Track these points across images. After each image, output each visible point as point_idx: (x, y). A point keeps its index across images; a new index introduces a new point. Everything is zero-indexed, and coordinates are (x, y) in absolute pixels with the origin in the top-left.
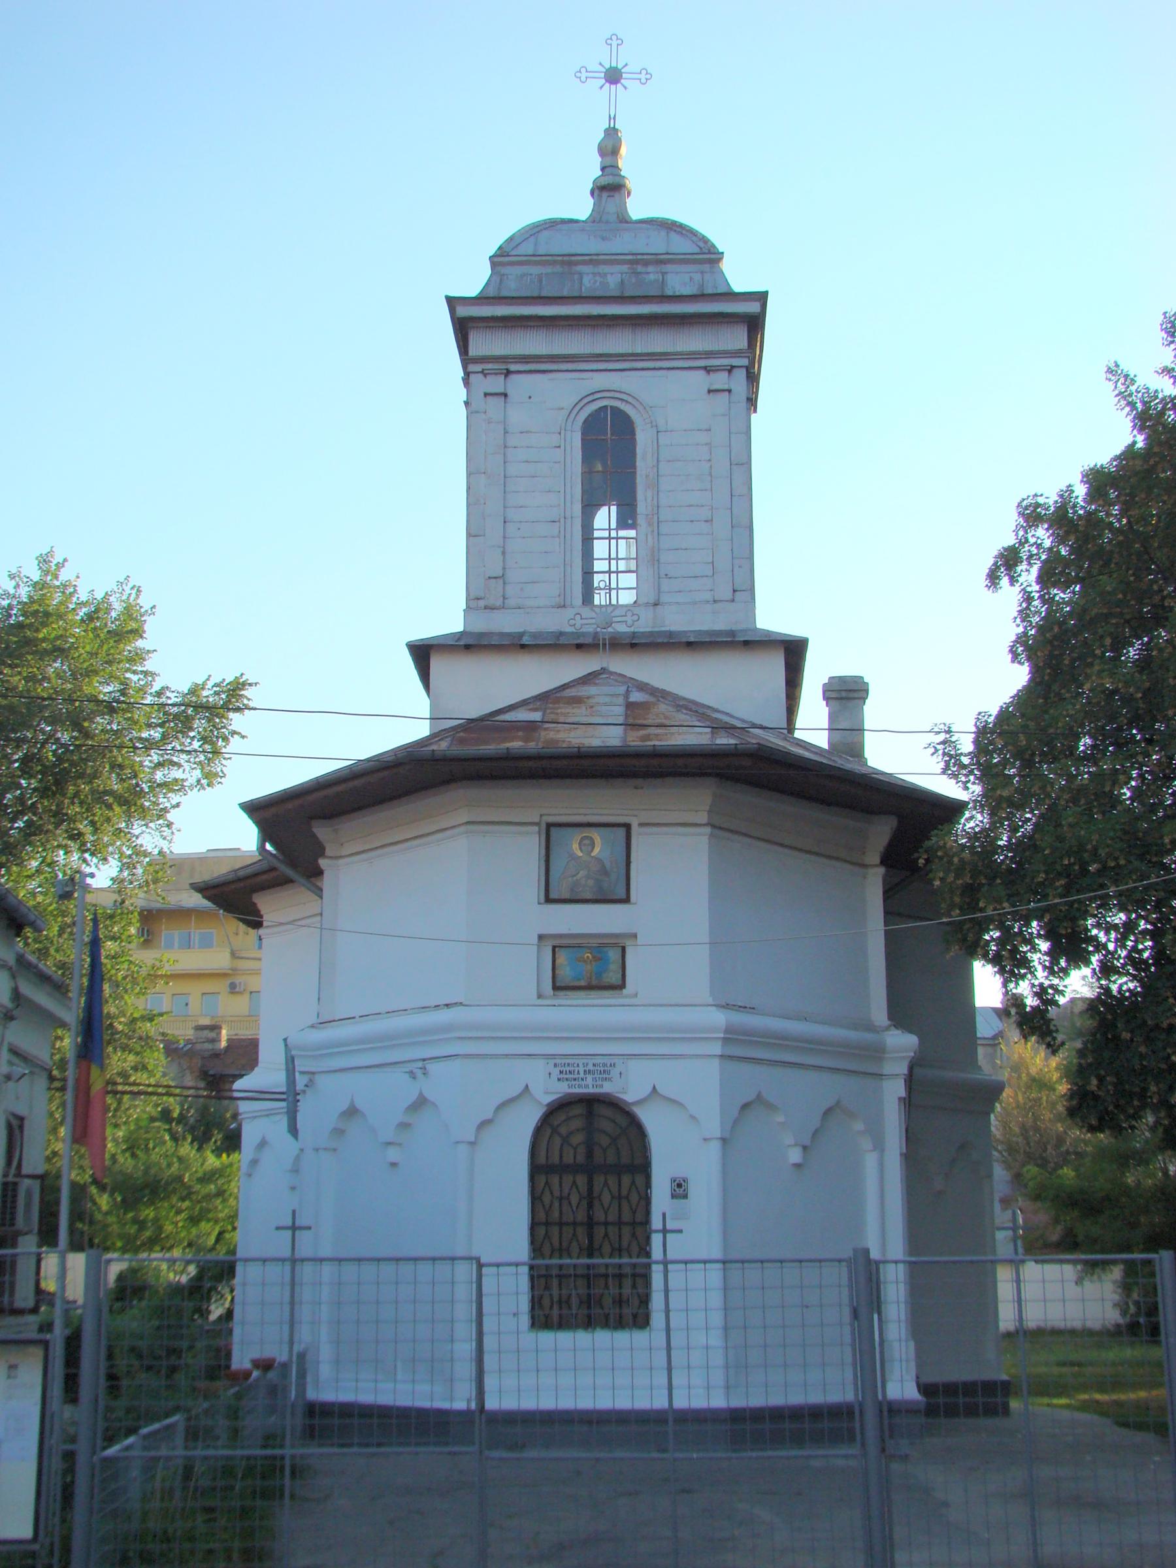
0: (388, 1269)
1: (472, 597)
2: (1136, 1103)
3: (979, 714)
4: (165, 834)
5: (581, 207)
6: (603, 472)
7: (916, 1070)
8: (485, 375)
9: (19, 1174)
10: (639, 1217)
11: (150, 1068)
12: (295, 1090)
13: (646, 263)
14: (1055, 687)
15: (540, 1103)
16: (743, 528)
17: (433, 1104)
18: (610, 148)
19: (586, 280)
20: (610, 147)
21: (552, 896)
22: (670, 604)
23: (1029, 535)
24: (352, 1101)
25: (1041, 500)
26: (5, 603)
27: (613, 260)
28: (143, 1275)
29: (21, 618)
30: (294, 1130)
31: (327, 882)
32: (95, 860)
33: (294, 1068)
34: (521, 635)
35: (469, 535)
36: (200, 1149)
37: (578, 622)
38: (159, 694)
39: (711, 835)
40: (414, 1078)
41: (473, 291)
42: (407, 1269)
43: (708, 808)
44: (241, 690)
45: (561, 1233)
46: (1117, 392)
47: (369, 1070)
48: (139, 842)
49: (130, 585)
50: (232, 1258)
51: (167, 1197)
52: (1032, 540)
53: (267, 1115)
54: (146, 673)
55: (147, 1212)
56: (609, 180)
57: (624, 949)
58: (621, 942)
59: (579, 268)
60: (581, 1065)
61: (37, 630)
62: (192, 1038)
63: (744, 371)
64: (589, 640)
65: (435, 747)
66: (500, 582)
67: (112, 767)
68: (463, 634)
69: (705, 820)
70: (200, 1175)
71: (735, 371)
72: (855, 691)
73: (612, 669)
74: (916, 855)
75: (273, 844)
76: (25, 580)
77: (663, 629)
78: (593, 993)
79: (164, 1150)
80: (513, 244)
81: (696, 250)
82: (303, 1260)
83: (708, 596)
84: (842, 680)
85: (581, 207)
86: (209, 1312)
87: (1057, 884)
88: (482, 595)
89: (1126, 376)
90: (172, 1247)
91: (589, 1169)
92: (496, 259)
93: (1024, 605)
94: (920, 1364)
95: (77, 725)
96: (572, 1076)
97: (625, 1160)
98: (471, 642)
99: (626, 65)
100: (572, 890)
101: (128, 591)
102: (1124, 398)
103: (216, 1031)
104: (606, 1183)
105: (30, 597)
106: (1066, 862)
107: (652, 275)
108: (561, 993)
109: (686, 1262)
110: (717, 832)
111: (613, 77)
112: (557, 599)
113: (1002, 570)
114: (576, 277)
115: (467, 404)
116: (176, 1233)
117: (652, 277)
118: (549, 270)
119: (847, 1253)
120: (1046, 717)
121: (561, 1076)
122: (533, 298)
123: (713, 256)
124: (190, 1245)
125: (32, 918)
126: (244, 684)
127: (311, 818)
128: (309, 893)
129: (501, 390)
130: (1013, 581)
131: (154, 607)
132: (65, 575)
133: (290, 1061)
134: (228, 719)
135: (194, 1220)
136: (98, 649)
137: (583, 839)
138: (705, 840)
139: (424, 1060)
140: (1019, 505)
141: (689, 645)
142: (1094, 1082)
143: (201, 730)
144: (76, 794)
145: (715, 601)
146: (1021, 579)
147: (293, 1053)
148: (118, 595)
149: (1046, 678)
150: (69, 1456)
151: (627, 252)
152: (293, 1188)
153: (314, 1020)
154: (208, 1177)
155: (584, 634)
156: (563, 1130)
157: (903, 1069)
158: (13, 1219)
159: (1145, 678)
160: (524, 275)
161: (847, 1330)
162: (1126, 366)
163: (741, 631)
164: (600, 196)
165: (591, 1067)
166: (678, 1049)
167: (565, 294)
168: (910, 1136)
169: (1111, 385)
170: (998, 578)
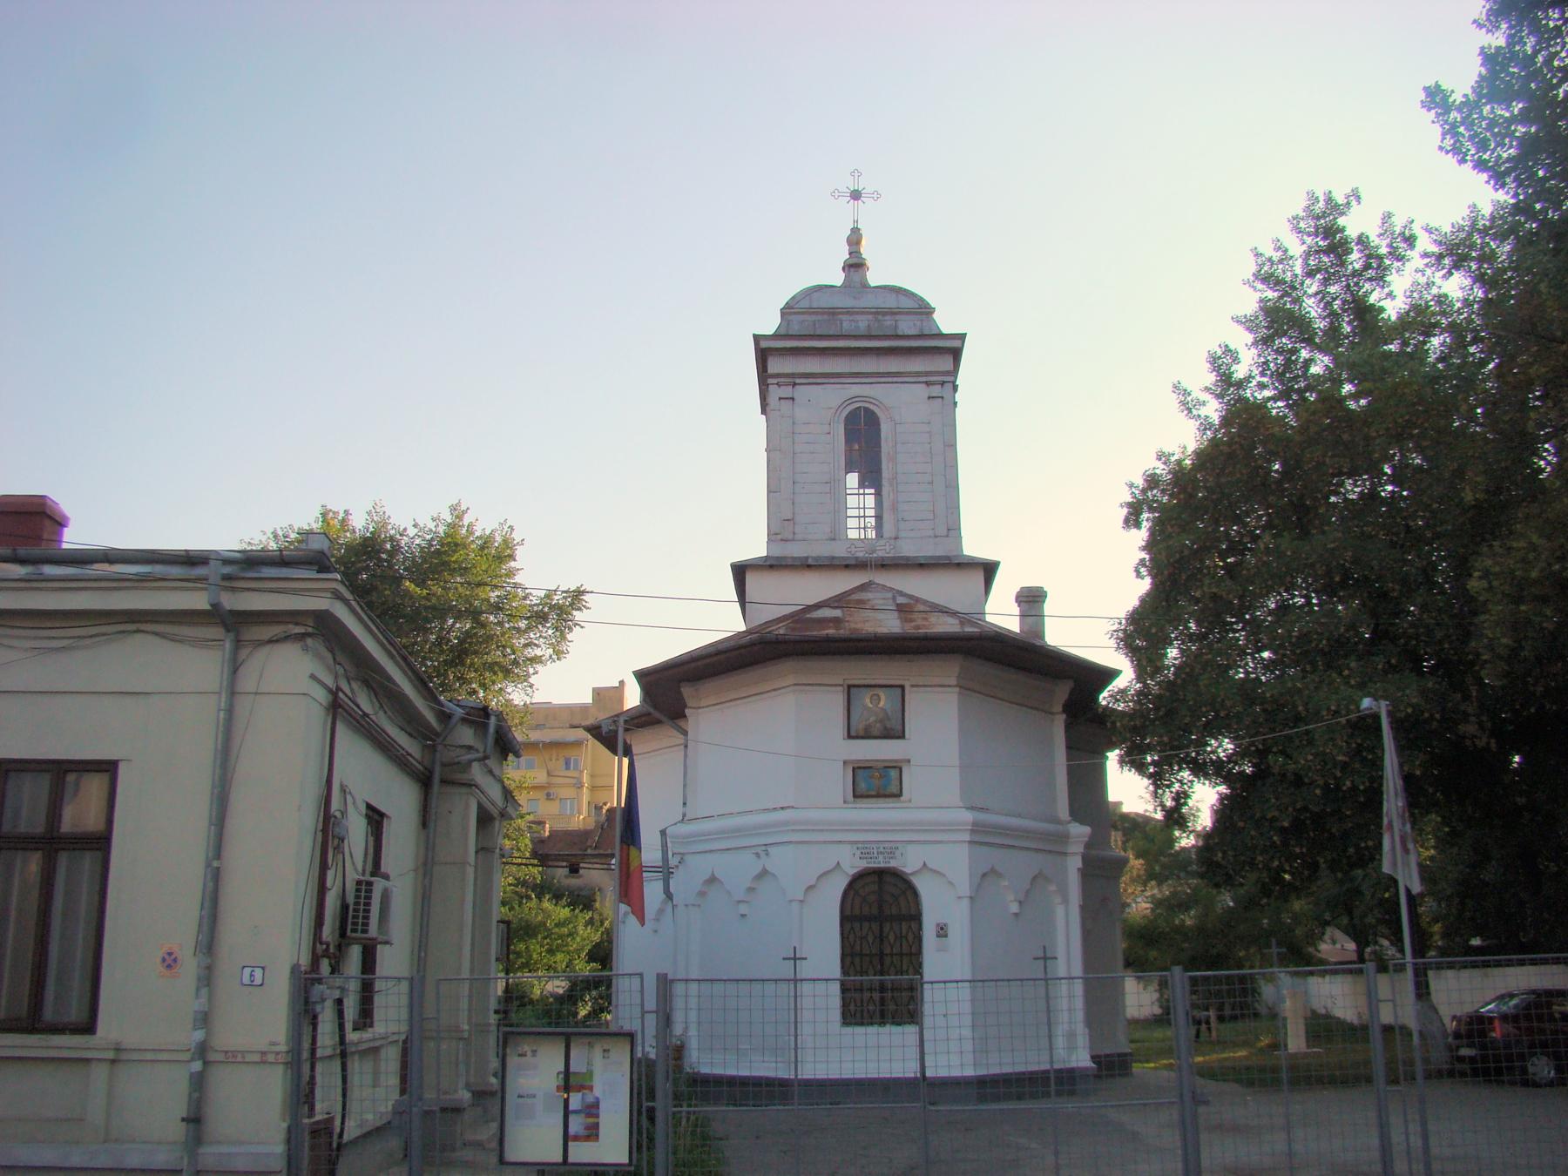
5: (838, 279)
8: (779, 386)
13: (885, 314)
15: (847, 874)
16: (952, 487)
17: (774, 875)
18: (855, 240)
19: (845, 324)
22: (906, 538)
24: (713, 874)
34: (807, 558)
35: (769, 492)
37: (853, 550)
39: (960, 693)
42: (757, 987)
45: (861, 962)
48: (511, 697)
58: (899, 764)
59: (840, 316)
67: (498, 647)
70: (556, 921)
71: (946, 385)
73: (877, 581)
78: (881, 800)
81: (917, 306)
83: (931, 533)
84: (1029, 589)
85: (838, 279)
86: (577, 1013)
88: (778, 531)
94: (1091, 1048)
98: (774, 563)
101: (506, 529)
102: (1184, 404)
104: (891, 928)
107: (888, 321)
109: (945, 982)
111: (856, 195)
117: (889, 323)
118: (820, 317)
127: (680, 682)
135: (551, 952)
142: (1220, 855)
145: (936, 537)
152: (656, 931)
164: (849, 271)
166: (940, 837)
167: (831, 333)
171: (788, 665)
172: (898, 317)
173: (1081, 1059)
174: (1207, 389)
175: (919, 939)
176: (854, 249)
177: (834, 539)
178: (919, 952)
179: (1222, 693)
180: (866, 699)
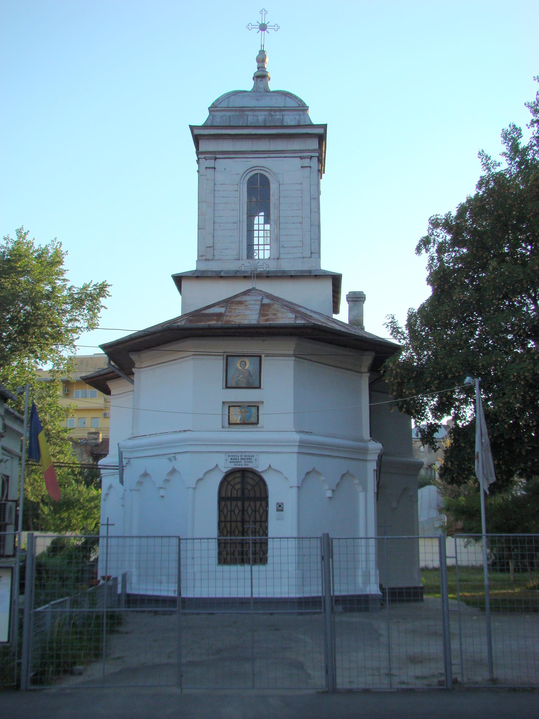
0: (158, 540)
1: (200, 255)
2: (466, 473)
3: (410, 309)
4: (73, 351)
5: (248, 85)
6: (256, 202)
7: (384, 458)
8: (206, 159)
9: (7, 500)
10: (263, 519)
11: (65, 452)
12: (122, 465)
13: (275, 111)
14: (442, 297)
18: (261, 59)
20: (261, 59)
21: (229, 385)
23: (434, 232)
24: (146, 471)
25: (439, 217)
26: (2, 250)
27: (261, 109)
28: (63, 541)
29: (9, 257)
30: (122, 482)
31: (136, 378)
32: (41, 362)
33: (122, 456)
34: (221, 271)
36: (88, 487)
38: (70, 289)
39: (295, 361)
40: (171, 461)
41: (201, 123)
42: (165, 540)
43: (293, 349)
44: (105, 288)
46: (482, 163)
47: (152, 458)
48: (61, 354)
49: (57, 242)
50: (97, 536)
51: (74, 507)
52: (435, 234)
53: (113, 475)
54: (64, 280)
55: (65, 514)
56: (261, 73)
57: (258, 407)
59: (247, 113)
60: (240, 456)
61: (16, 263)
62: (87, 437)
63: (317, 158)
64: (249, 275)
65: (179, 324)
66: (212, 248)
68: (195, 271)
69: (292, 352)
70: (88, 498)
71: (313, 158)
72: (359, 298)
73: (257, 288)
74: (379, 369)
75: (114, 362)
76: (11, 240)
77: (281, 269)
78: (246, 426)
79: (72, 488)
80: (219, 102)
81: (297, 105)
82: (111, 537)
83: (300, 255)
84: (354, 293)
85: (248, 85)
86: (90, 557)
87: (435, 382)
88: (204, 254)
89: (487, 156)
90: (75, 529)
91: (243, 498)
92: (211, 109)
93: (431, 262)
95: (33, 304)
96: (236, 461)
97: (258, 495)
98: (199, 275)
99: (269, 22)
100: (237, 383)
103: (97, 435)
105: (13, 248)
106: (439, 373)
108: (232, 426)
110: (297, 359)
111: (263, 28)
112: (236, 256)
113: (423, 246)
114: (245, 117)
115: (198, 171)
116: (78, 523)
117: (278, 117)
118: (234, 113)
119: (320, 535)
120: (437, 310)
121: (231, 461)
122: (226, 126)
123: (304, 108)
124: (83, 529)
125: (11, 395)
126: (106, 285)
127: (129, 351)
128: (128, 382)
129: (213, 166)
130: (427, 250)
131: (67, 251)
132: (29, 238)
133: (121, 454)
134: (99, 301)
135: (85, 518)
136: (43, 270)
137: (241, 362)
138: (292, 362)
139: (175, 453)
140: (430, 219)
141: (292, 277)
143: (88, 305)
144: (34, 333)
145: (303, 258)
146: (431, 250)
147: (121, 450)
148: (52, 246)
149: (439, 293)
150: (21, 611)
151: (267, 106)
152: (123, 506)
153: (130, 436)
154: (92, 499)
155: (247, 272)
156: (232, 483)
157: (376, 457)
158: (4, 518)
159: (477, 295)
160: (222, 116)
161: (319, 564)
162: (487, 152)
163: (314, 270)
164: (257, 80)
165: (243, 457)
167: (241, 124)
168: (379, 486)
169: (480, 160)
170: (421, 249)
171: (189, 344)
172: (285, 113)
173: (373, 589)
174: (504, 154)
175: (267, 512)
176: (260, 65)
177: (239, 259)
178: (266, 521)
179: (451, 363)
180: (237, 364)
